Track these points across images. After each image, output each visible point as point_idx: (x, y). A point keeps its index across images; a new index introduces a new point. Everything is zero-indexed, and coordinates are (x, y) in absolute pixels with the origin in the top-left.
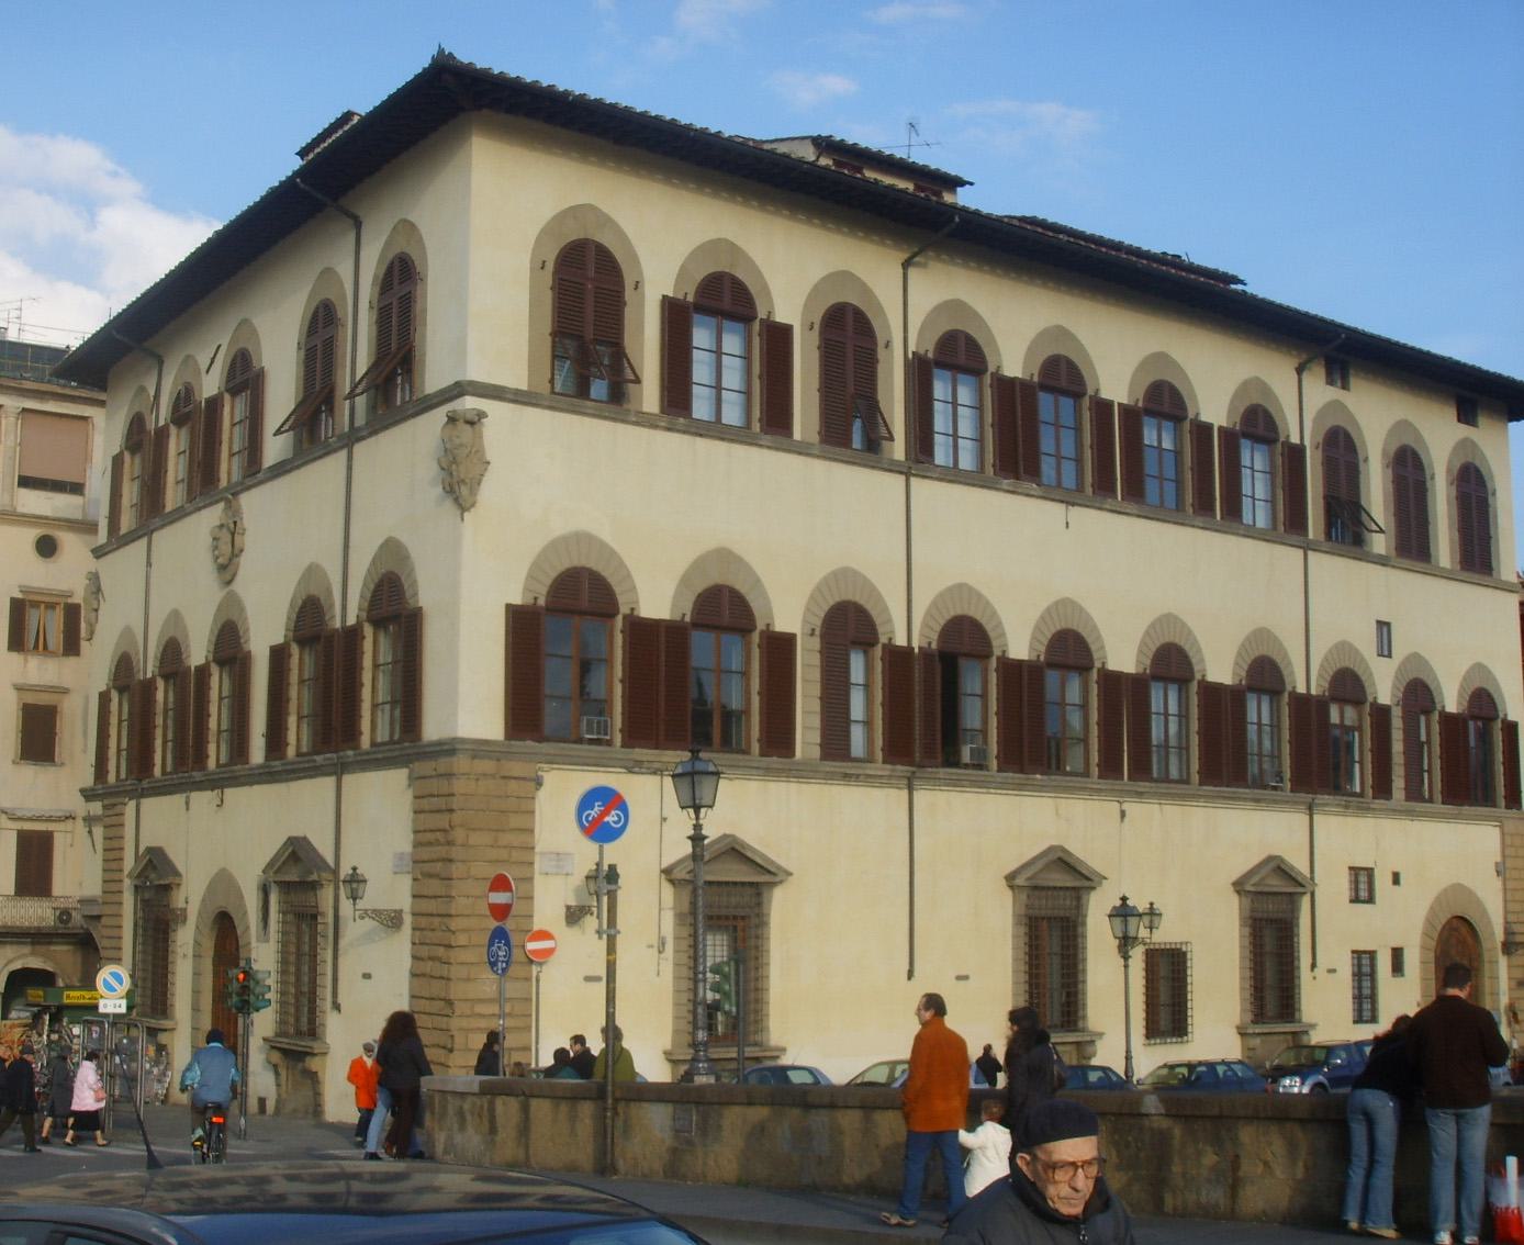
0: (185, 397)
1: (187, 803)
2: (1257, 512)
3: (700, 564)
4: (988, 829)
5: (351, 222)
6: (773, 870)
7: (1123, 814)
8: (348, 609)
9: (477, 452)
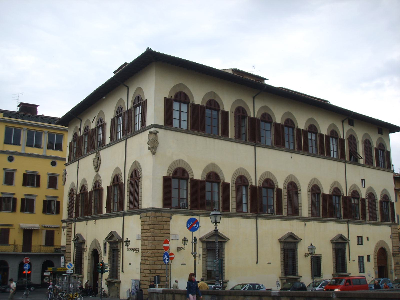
0: (87, 128)
1: (87, 223)
4: (274, 229)
7: (305, 225)
8: (126, 179)
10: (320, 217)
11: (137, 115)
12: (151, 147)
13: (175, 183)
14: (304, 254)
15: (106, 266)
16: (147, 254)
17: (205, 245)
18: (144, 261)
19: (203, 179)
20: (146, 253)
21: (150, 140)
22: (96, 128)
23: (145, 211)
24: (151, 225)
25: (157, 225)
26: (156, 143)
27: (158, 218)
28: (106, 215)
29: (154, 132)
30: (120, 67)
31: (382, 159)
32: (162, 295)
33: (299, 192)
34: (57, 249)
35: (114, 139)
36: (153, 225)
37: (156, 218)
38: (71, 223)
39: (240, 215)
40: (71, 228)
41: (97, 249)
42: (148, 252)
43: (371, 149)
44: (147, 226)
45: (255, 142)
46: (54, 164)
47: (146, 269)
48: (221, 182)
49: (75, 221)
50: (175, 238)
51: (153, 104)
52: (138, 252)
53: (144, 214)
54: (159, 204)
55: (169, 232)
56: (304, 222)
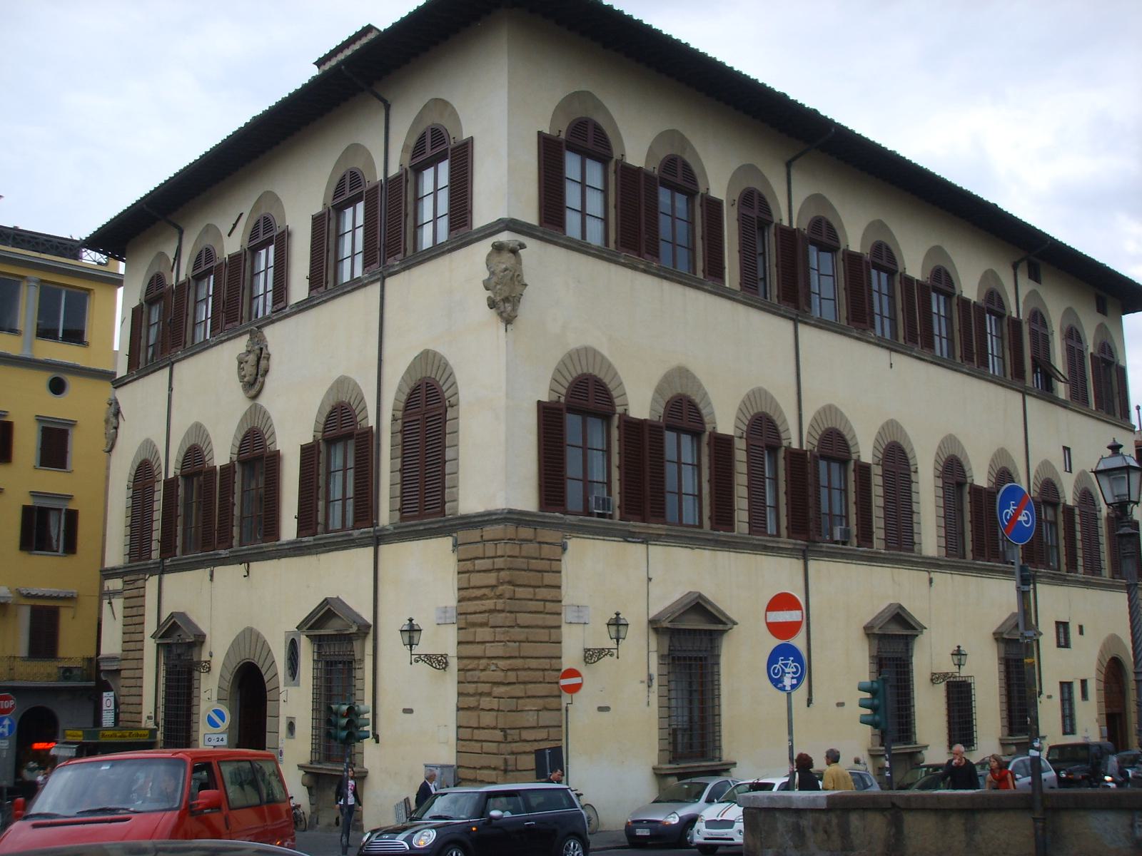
0: (205, 257)
1: (212, 576)
2: (994, 366)
3: (667, 379)
4: (848, 595)
5: (381, 104)
6: (724, 620)
7: (931, 581)
8: (382, 414)
9: (518, 275)
10: (964, 557)
11: (259, 273)
12: (498, 299)
13: (573, 423)
14: (928, 677)
15: (361, 716)
16: (484, 673)
17: (666, 642)
18: (472, 699)
19: (655, 420)
20: (482, 670)
21: (497, 271)
22: (245, 252)
23: (475, 522)
24: (503, 569)
25: (523, 573)
26: (516, 283)
27: (525, 546)
28: (297, 543)
29: (511, 245)
30: (357, 33)
31: (1102, 387)
32: (824, 818)
33: (913, 477)
34: (68, 670)
35: (327, 283)
36: (511, 572)
37: (520, 548)
38: (141, 576)
39: (760, 543)
40: (143, 596)
41: (255, 661)
42: (493, 667)
43: (1081, 353)
44: (482, 574)
45: (797, 308)
46: (57, 387)
47: (484, 728)
48: (707, 433)
49: (161, 570)
50: (578, 617)
51: (504, 151)
52: (444, 669)
53: (463, 535)
54: (526, 499)
55: (561, 594)
56: (927, 573)
